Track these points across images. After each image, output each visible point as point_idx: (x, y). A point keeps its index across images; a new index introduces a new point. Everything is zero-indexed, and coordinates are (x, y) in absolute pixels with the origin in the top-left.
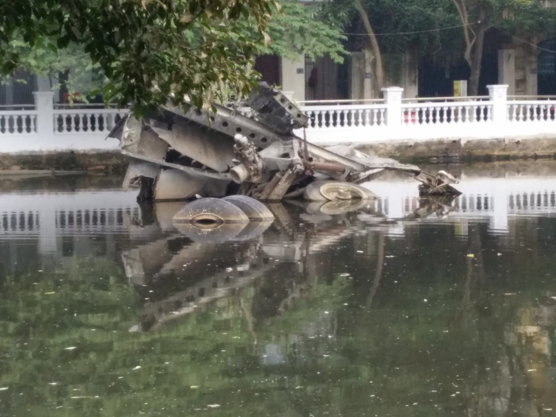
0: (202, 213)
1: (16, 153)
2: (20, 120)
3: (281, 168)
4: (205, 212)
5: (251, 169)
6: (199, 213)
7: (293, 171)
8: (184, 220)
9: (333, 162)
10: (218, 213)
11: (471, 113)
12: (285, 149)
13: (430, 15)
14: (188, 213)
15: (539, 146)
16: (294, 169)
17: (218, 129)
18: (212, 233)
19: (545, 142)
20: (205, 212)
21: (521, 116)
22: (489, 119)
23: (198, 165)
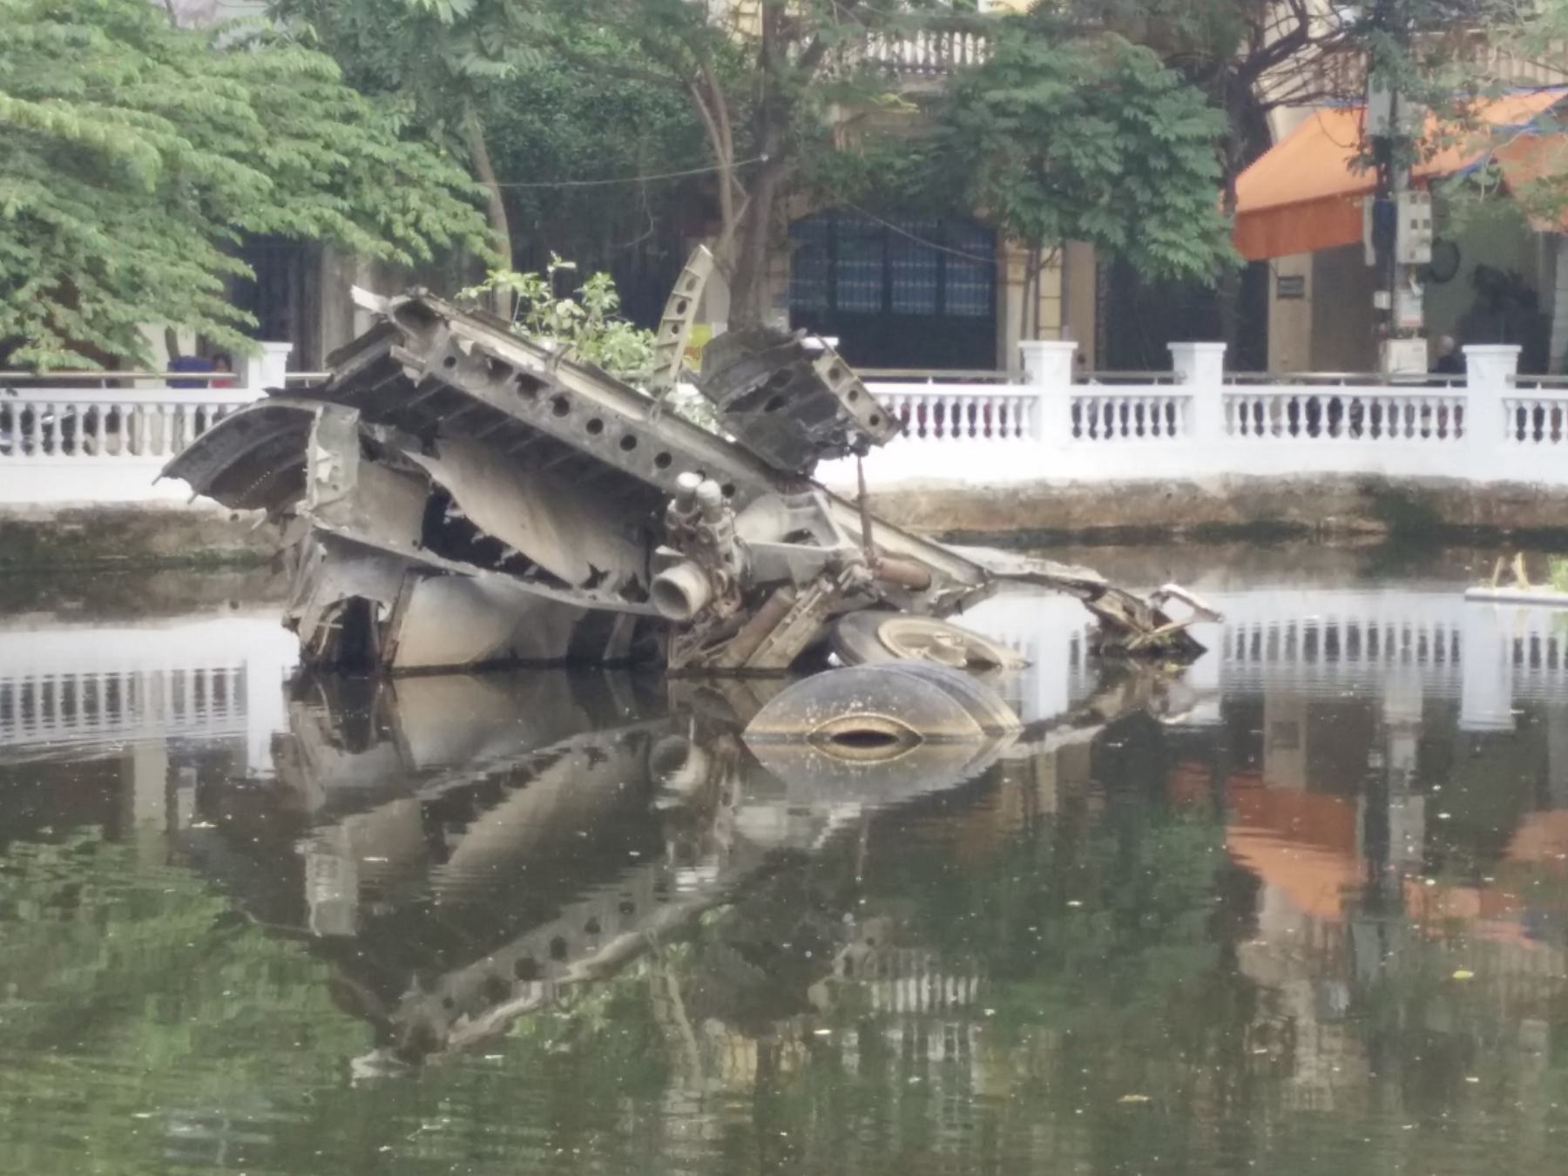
0: (848, 714)
1: (33, 506)
2: (1335, 407)
3: (798, 575)
4: (856, 710)
5: (720, 578)
6: (837, 713)
7: (837, 585)
8: (793, 735)
9: (910, 558)
10: (900, 713)
11: (1275, 413)
12: (795, 517)
13: (541, 132)
14: (803, 714)
15: (909, 514)
16: (841, 579)
17: (607, 457)
18: (880, 772)
19: (923, 500)
20: (856, 710)
21: (1101, 427)
22: (1179, 433)
23: (519, 566)
